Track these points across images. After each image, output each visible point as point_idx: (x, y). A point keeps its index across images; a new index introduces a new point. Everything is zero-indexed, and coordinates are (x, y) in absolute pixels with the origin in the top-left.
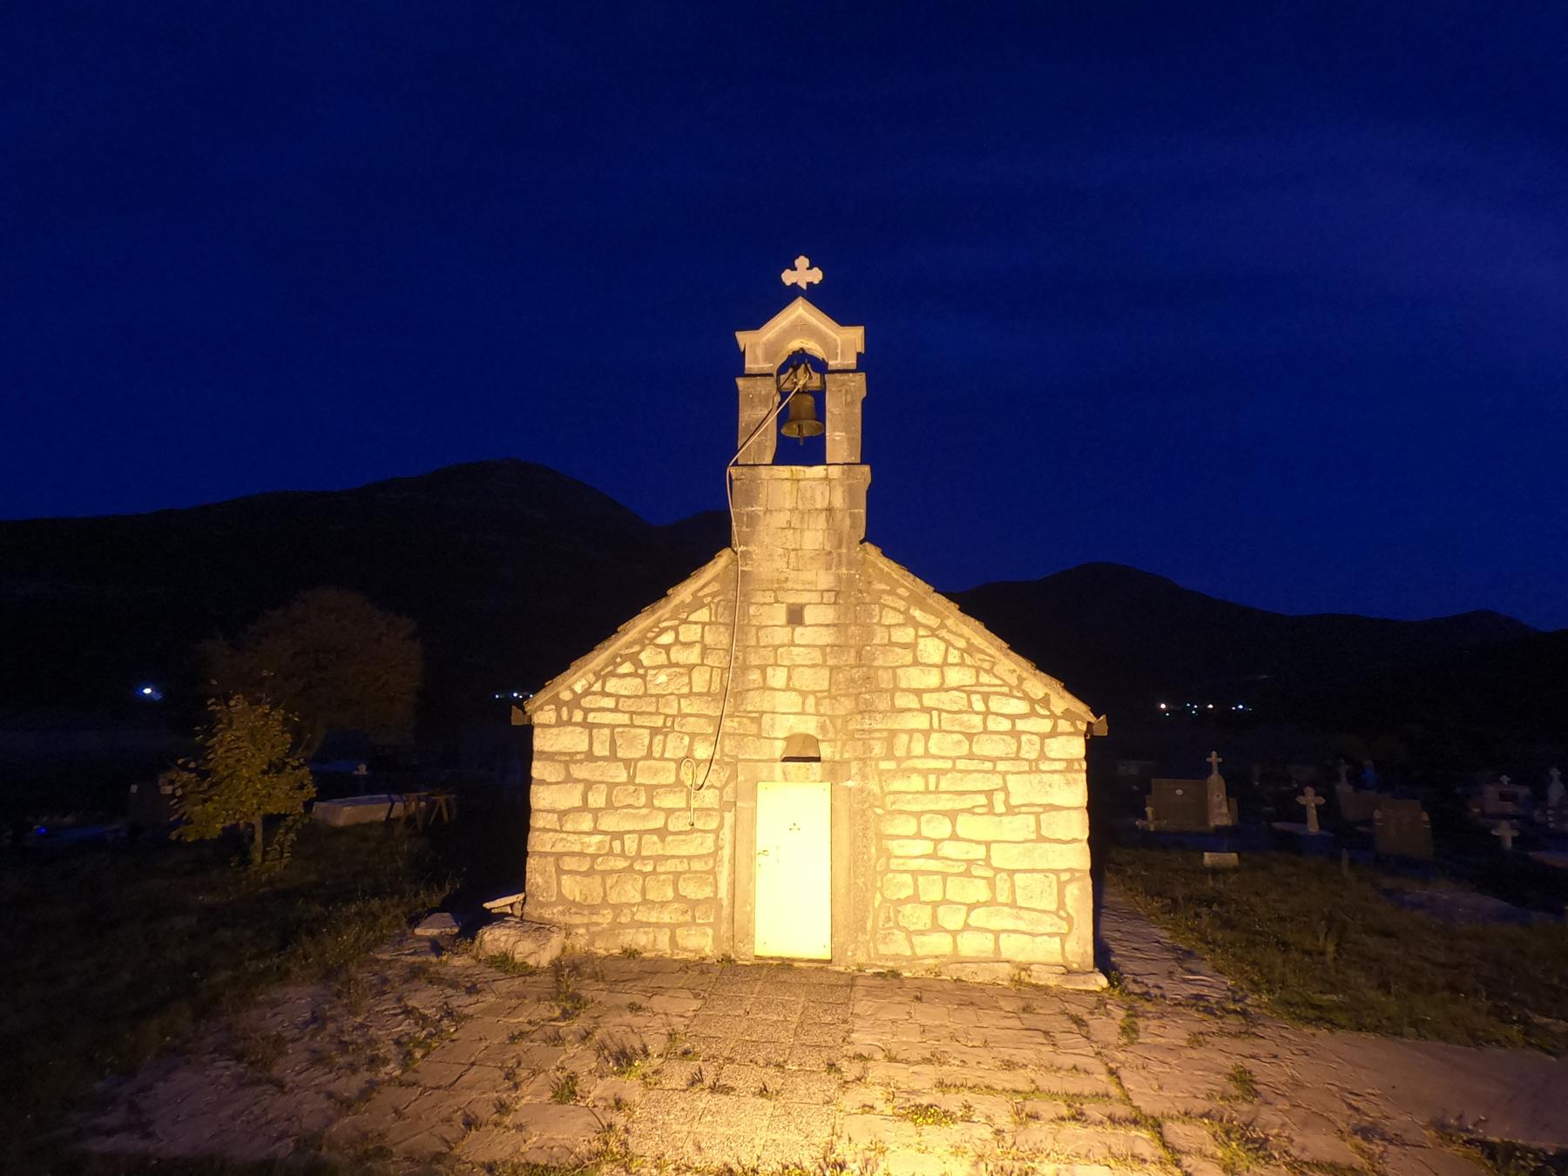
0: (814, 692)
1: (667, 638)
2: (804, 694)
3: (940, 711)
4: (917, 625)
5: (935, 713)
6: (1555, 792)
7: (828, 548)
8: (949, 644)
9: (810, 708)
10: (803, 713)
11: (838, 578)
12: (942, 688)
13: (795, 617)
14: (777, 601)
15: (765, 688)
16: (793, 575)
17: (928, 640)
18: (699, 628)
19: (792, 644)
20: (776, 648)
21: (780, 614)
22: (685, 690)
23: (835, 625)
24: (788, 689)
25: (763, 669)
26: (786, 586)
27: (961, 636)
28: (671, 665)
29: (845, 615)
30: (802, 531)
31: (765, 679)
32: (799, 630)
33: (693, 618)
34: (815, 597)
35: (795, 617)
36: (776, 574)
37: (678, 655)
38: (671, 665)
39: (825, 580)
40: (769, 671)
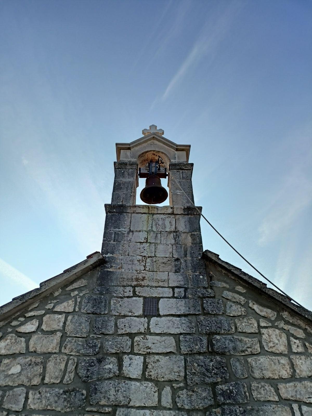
0: (170, 381)
1: (30, 327)
2: (159, 384)
3: (300, 403)
4: (258, 317)
5: (295, 407)
6: (229, 415)
7: (176, 256)
8: (289, 335)
9: (167, 400)
10: (159, 407)
11: (186, 279)
12: (293, 378)
13: (151, 308)
14: (135, 295)
15: (120, 376)
16: (148, 275)
17: (270, 331)
18: (62, 318)
19: (148, 332)
20: (131, 336)
21: (138, 306)
22: (36, 381)
23: (185, 316)
24: (144, 378)
25: (119, 357)
26: (143, 283)
27: (299, 327)
28: (28, 352)
29: (194, 306)
30: (156, 244)
31: (120, 366)
32: (154, 320)
33: (58, 309)
34: (168, 292)
35: (151, 308)
36: (135, 275)
37: (37, 343)
38: (28, 352)
39: (175, 279)
40: (126, 358)
